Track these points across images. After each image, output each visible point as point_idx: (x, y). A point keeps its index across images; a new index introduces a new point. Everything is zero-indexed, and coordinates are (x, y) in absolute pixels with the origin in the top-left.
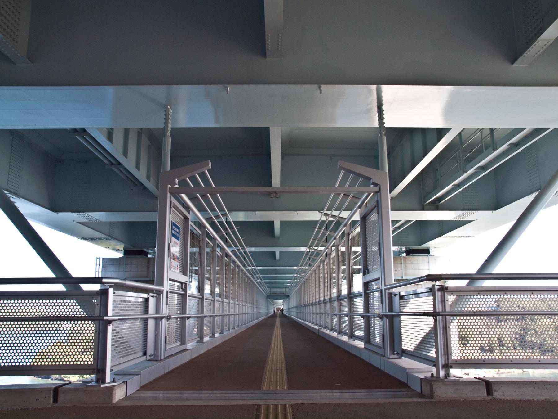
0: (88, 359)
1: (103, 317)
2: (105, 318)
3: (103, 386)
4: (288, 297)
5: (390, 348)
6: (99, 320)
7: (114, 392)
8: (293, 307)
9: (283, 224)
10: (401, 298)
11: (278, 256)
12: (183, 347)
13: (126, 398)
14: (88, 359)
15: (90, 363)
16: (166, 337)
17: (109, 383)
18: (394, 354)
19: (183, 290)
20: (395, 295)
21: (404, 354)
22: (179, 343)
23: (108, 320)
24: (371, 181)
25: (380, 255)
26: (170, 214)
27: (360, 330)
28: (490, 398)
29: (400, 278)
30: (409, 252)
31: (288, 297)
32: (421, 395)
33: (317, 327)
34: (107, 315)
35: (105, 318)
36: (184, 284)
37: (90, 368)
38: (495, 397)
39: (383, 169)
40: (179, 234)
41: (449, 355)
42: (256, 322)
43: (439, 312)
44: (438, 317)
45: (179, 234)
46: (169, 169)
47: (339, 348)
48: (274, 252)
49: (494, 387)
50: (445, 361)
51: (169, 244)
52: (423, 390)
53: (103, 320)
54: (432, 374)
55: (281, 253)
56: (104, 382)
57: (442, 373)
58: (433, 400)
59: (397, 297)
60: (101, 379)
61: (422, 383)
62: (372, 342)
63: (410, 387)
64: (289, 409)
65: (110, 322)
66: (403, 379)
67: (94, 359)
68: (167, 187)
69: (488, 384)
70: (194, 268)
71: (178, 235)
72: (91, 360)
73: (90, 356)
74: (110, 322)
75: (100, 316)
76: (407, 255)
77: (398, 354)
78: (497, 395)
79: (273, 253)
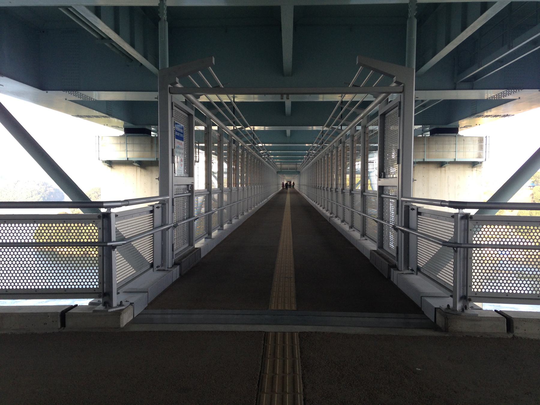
0: (93, 283)
1: (107, 243)
2: (108, 244)
3: (110, 310)
4: (299, 173)
5: (404, 264)
6: (103, 246)
7: (121, 317)
8: (304, 185)
9: (294, 104)
10: (419, 213)
11: (288, 133)
12: (191, 248)
13: (134, 321)
14: (93, 283)
15: (95, 287)
16: (173, 245)
17: (116, 307)
18: (408, 269)
19: (190, 192)
20: (413, 209)
21: (419, 273)
22: (187, 245)
23: (111, 246)
24: (395, 79)
25: (399, 116)
26: (172, 116)
27: (374, 208)
28: (510, 336)
29: (422, 160)
30: (433, 132)
31: (299, 173)
32: (434, 326)
33: (328, 214)
34: (110, 241)
35: (108, 244)
36: (190, 186)
37: (97, 291)
38: (516, 335)
39: (410, 66)
40: (183, 134)
41: (469, 288)
42: (265, 201)
43: (461, 244)
44: (458, 249)
45: (183, 134)
46: (168, 66)
47: (352, 246)
48: (285, 131)
49: (515, 324)
50: (463, 293)
51: (173, 150)
52: (437, 320)
53: (107, 246)
54: (448, 306)
55: (292, 132)
56: (111, 306)
57: (459, 306)
58: (447, 335)
59: (415, 212)
60: (108, 304)
61: (437, 313)
62: (385, 247)
63: (423, 313)
64: (296, 336)
65: (114, 247)
66: (417, 302)
67: (100, 283)
68: (167, 86)
69: (508, 320)
70: (200, 145)
71: (181, 135)
72: (97, 283)
73: (95, 280)
74: (114, 247)
75: (103, 242)
76: (431, 134)
77: (412, 270)
78: (518, 332)
79: (285, 132)
